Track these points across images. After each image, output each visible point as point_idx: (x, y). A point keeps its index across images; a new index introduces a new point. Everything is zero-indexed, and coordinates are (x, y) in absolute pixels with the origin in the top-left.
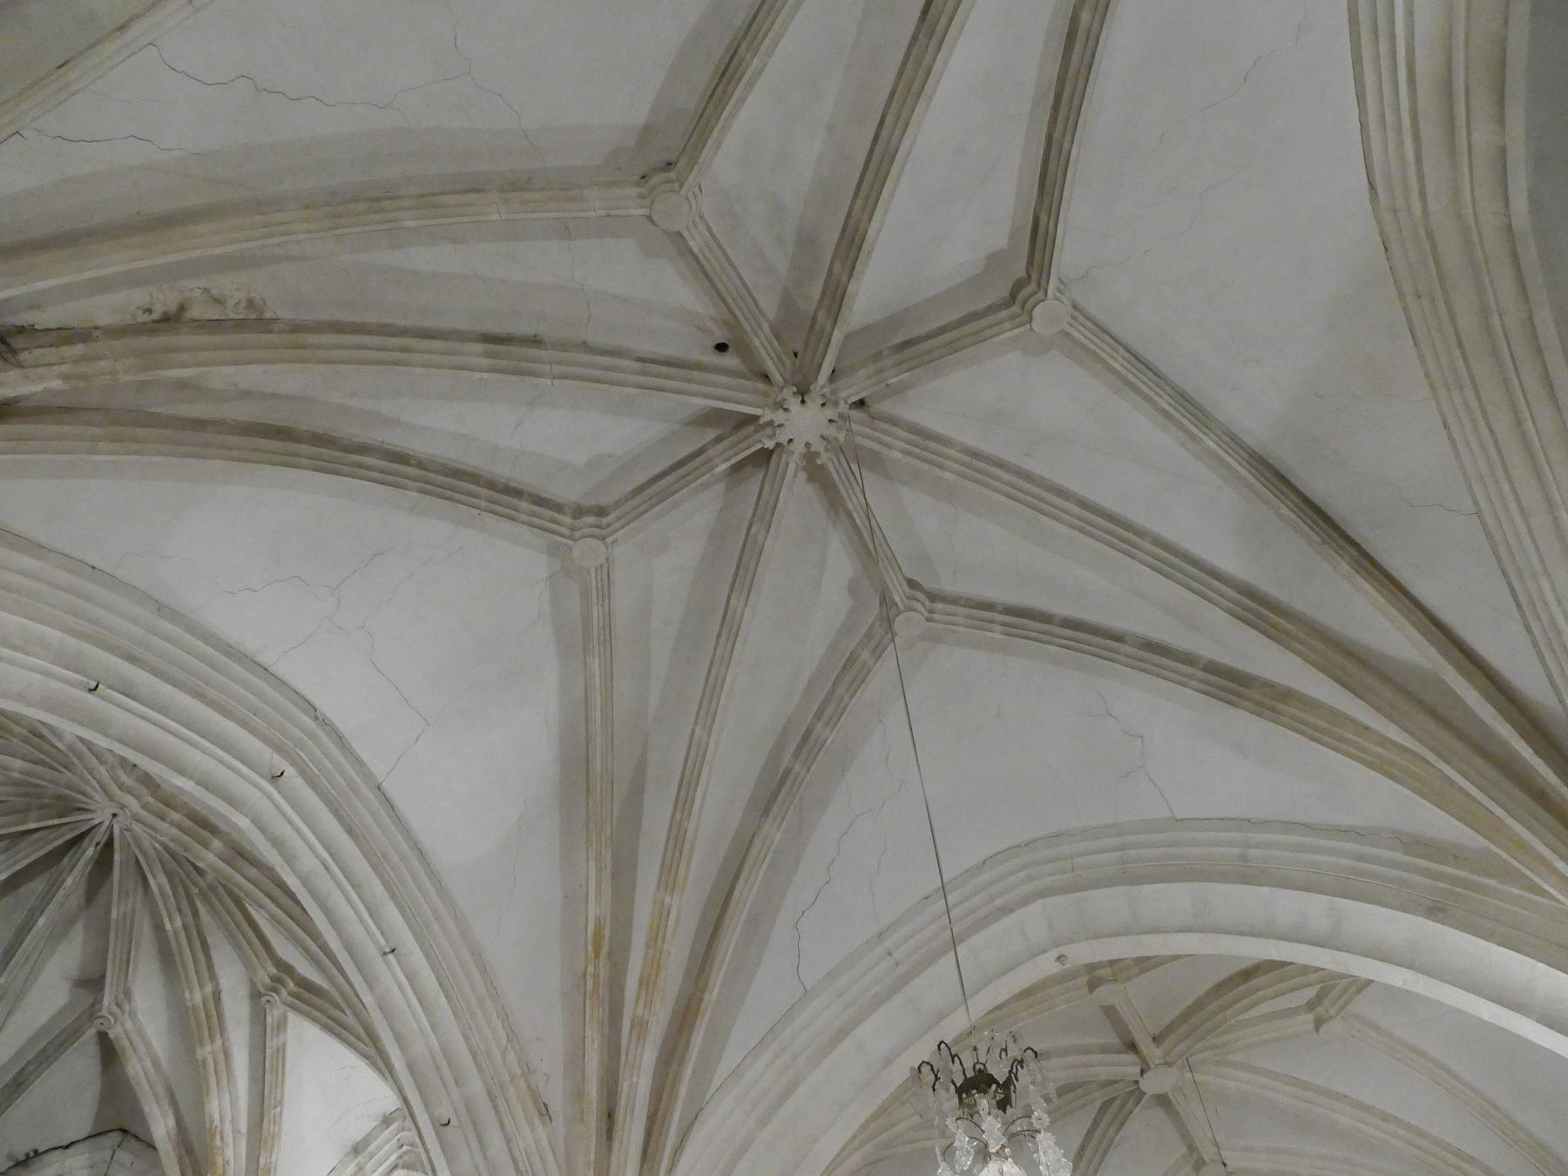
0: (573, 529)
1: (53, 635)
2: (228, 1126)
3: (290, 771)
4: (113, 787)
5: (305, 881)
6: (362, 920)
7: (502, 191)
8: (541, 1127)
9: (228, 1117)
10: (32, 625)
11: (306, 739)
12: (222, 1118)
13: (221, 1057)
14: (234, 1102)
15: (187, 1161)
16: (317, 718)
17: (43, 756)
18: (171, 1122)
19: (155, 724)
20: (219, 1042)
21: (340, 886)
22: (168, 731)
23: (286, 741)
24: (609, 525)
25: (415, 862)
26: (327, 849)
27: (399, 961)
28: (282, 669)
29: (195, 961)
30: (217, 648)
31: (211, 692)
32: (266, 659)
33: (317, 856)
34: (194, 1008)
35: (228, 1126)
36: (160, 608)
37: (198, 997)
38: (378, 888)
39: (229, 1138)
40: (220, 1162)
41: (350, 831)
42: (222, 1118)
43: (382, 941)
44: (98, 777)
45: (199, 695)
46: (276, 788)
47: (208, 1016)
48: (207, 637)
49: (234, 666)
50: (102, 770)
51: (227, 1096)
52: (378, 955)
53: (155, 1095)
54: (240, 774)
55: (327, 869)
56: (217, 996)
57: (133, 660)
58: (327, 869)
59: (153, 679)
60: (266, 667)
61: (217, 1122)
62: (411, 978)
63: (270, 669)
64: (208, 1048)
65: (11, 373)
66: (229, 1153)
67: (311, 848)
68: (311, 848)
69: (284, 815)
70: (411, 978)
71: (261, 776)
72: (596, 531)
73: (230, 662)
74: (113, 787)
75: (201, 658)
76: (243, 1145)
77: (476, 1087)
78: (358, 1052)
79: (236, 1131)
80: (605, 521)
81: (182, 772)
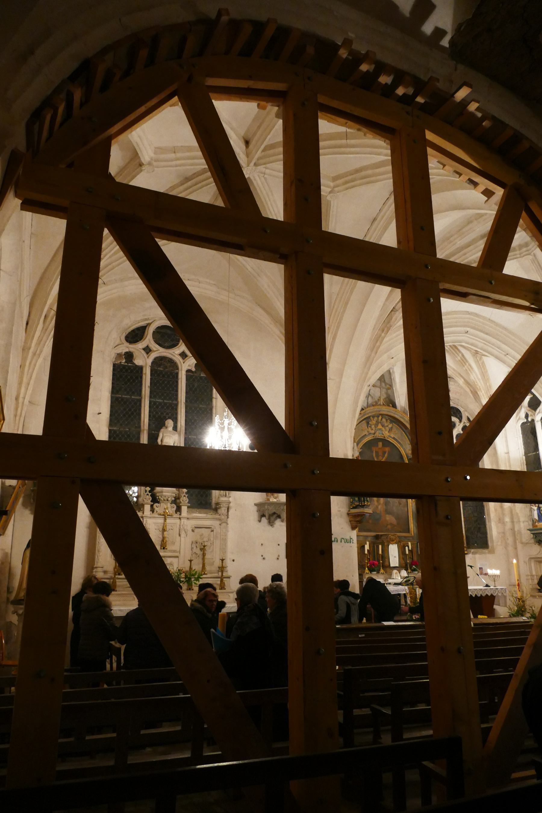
0: (520, 254)
2: (477, 379)
3: (468, 329)
7: (476, 219)
9: (476, 377)
11: (469, 320)
12: (475, 378)
13: (469, 367)
14: (476, 375)
15: (469, 386)
16: (469, 314)
18: (463, 380)
20: (467, 364)
24: (530, 249)
25: (504, 332)
29: (455, 351)
33: (482, 343)
34: (459, 360)
35: (477, 379)
37: (459, 358)
38: (498, 342)
39: (478, 382)
40: (478, 387)
41: (487, 334)
42: (475, 378)
43: (504, 353)
47: (463, 361)
51: (474, 374)
53: (457, 376)
54: (459, 336)
55: (485, 344)
56: (463, 355)
58: (485, 344)
61: (474, 380)
64: (466, 367)
65: (397, 313)
66: (480, 385)
67: (480, 342)
68: (480, 342)
69: (471, 338)
71: (463, 334)
72: (527, 252)
76: (482, 381)
79: (479, 379)
80: (529, 248)
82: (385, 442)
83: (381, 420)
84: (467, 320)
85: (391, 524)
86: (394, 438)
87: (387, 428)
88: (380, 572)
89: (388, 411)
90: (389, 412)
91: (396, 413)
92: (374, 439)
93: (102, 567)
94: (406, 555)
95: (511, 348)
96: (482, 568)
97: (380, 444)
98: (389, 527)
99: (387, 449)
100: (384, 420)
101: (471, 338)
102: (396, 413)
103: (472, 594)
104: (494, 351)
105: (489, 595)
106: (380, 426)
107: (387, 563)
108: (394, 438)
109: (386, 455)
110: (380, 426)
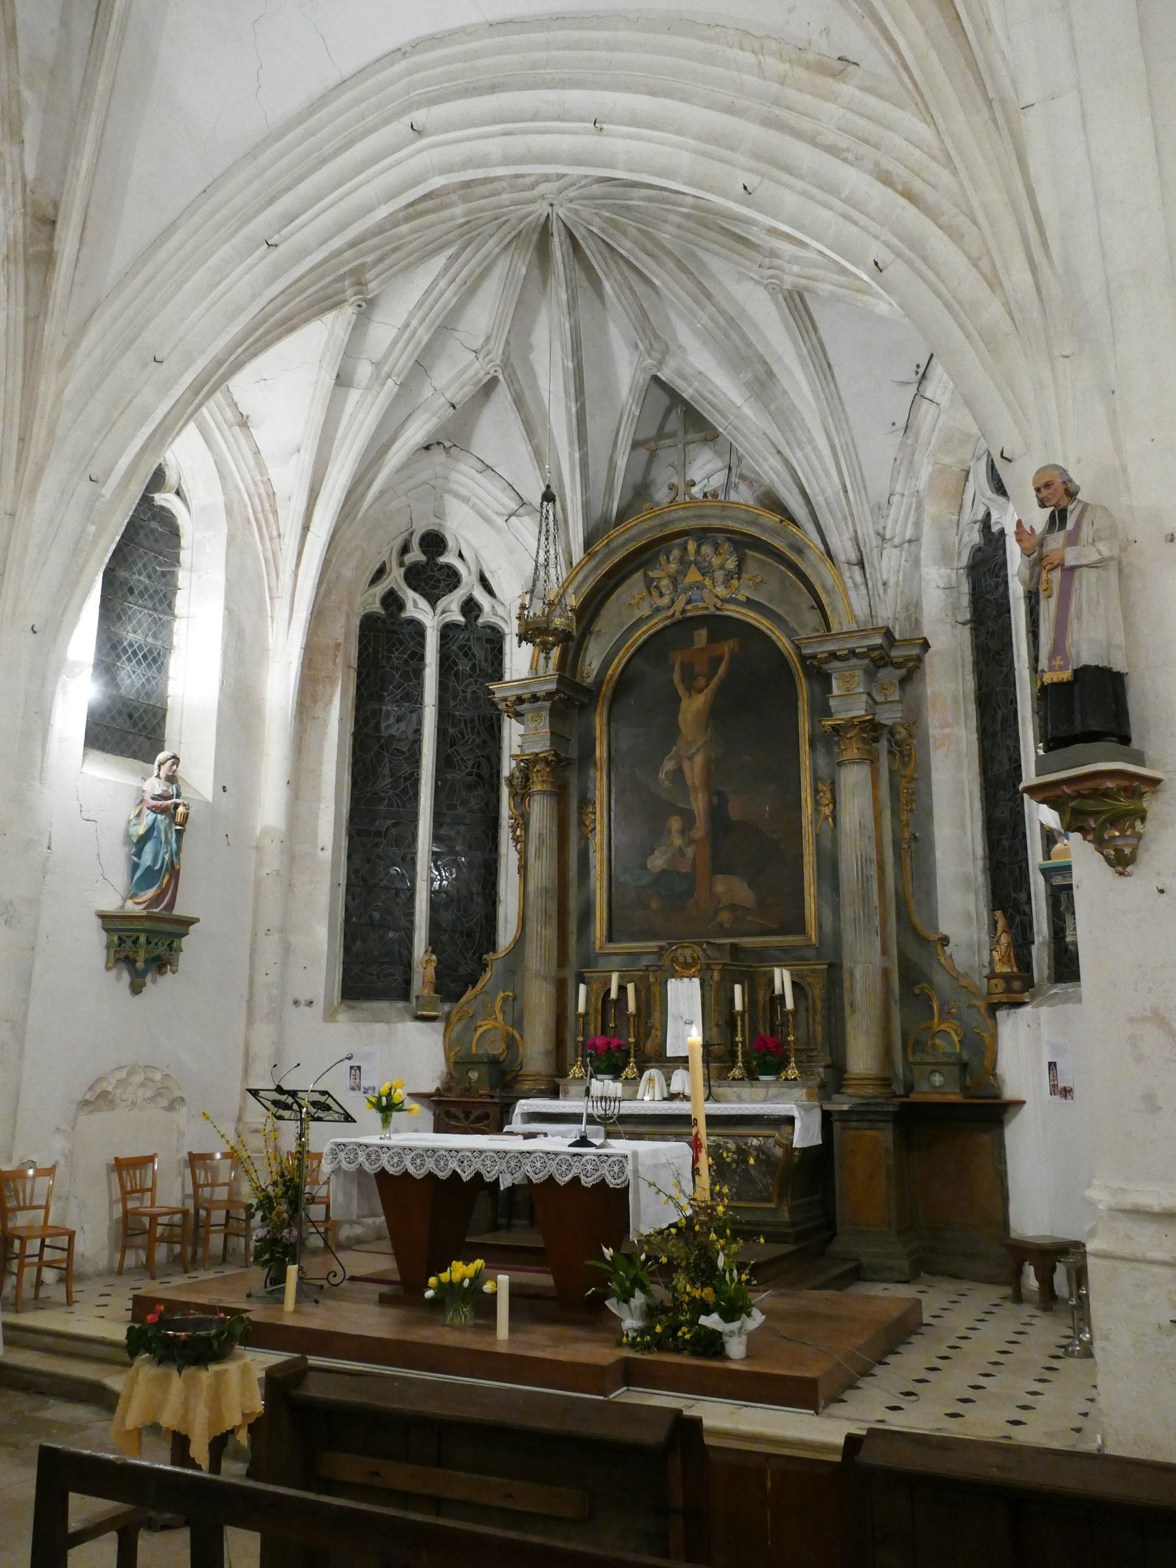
1: (225, 251)
3: (419, 116)
4: (528, 194)
5: (507, 161)
6: (563, 132)
8: (843, 85)
10: (210, 263)
17: (467, 236)
19: (316, 217)
21: (525, 132)
22: (337, 202)
23: (401, 100)
25: (561, 35)
26: (494, 122)
27: (611, 122)
28: (349, 64)
30: (301, 122)
31: (328, 149)
32: (333, 78)
36: (252, 154)
41: (493, 89)
44: (508, 203)
45: (324, 161)
46: (432, 135)
48: (289, 126)
49: (323, 113)
50: (505, 196)
52: (595, 138)
54: (360, 185)
57: (272, 201)
59: (291, 194)
60: (340, 81)
62: (634, 121)
63: (345, 78)
69: (449, 143)
70: (634, 121)
73: (317, 116)
74: (528, 194)
75: (301, 141)
77: (752, 131)
78: (260, 352)
81: (371, 209)
82: (719, 626)
83: (698, 551)
84: (439, 70)
85: (733, 907)
86: (750, 603)
87: (719, 575)
88: (623, 1075)
89: (695, 517)
90: (701, 517)
91: (725, 513)
92: (673, 624)
93: (350, 1058)
94: (628, 1017)
95: (604, 87)
96: (1055, 1064)
97: (701, 636)
98: (724, 916)
99: (727, 648)
100: (706, 550)
101: (449, 143)
102: (725, 513)
103: (459, 1171)
104: (548, 138)
105: (563, 1180)
106: (693, 576)
107: (649, 1046)
108: (750, 603)
109: (722, 670)
110: (693, 576)
